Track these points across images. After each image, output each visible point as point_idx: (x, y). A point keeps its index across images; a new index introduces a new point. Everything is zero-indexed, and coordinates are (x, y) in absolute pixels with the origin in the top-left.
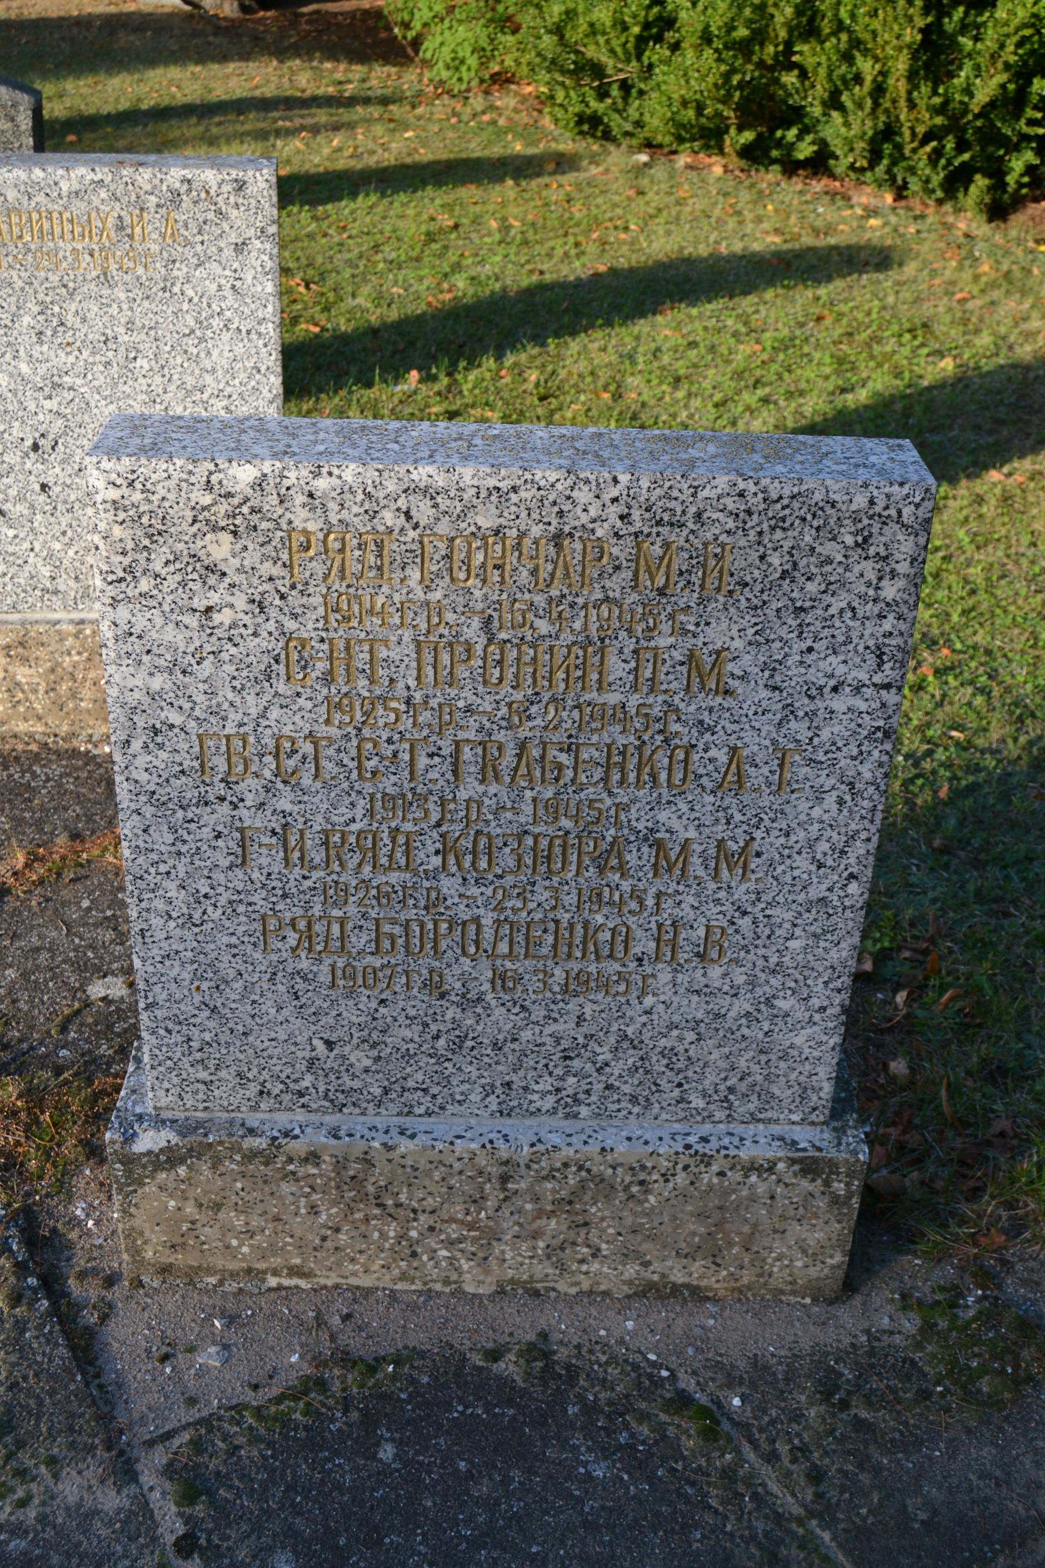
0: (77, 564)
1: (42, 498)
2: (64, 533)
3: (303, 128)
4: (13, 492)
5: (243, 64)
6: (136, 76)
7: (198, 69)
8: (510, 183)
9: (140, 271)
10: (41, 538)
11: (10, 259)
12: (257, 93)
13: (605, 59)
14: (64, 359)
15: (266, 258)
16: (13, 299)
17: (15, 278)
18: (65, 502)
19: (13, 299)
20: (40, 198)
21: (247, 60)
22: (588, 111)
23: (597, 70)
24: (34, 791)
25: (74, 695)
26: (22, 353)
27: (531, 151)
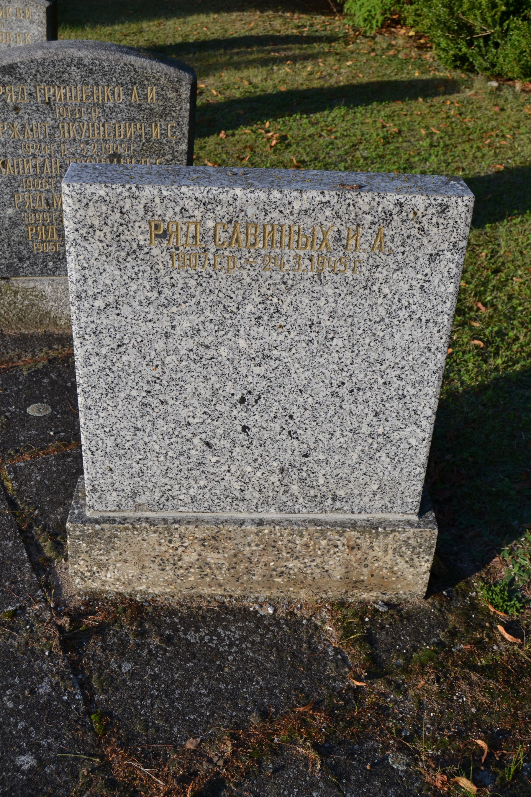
0: (262, 482)
1: (243, 436)
2: (255, 461)
3: (287, 58)
4: (219, 432)
5: (241, 14)
6: (182, 20)
7: (216, 16)
8: (421, 100)
9: (349, 273)
10: (237, 463)
11: (243, 261)
12: (253, 33)
13: (478, 24)
14: (275, 337)
15: (453, 266)
16: (241, 292)
17: (245, 276)
18: (260, 439)
19: (241, 292)
20: (275, 215)
21: (243, 11)
22: (460, 54)
23: (470, 29)
24: (222, 656)
25: (248, 571)
26: (242, 332)
27: (425, 77)
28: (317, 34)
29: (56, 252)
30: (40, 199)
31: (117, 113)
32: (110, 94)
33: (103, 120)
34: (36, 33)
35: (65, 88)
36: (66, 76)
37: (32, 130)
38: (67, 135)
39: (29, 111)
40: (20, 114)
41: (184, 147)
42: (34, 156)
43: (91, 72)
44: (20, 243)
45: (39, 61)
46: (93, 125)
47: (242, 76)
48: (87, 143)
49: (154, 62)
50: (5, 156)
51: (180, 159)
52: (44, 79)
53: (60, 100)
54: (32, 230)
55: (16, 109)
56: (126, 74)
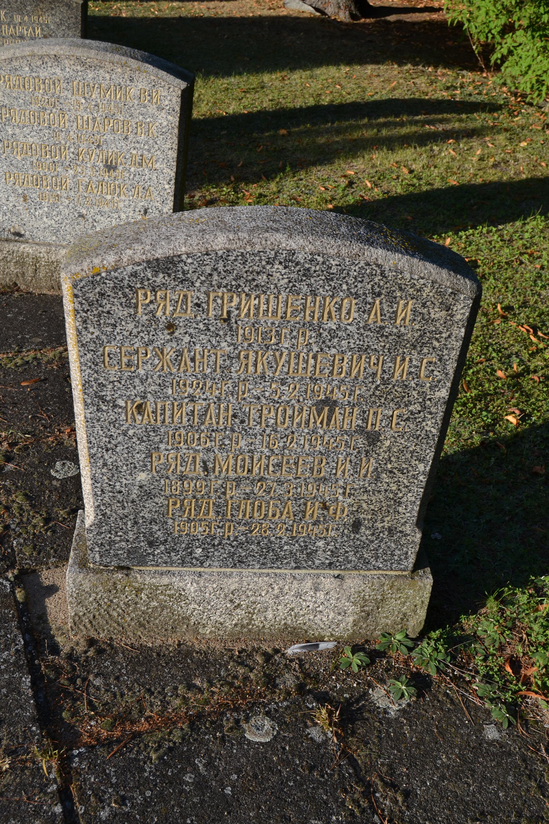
5: (376, 67)
6: (308, 72)
28: (472, 99)
29: (209, 535)
30: (195, 462)
31: (341, 339)
32: (333, 309)
33: (315, 349)
34: (165, 124)
35: (258, 297)
36: (262, 279)
37: (193, 360)
38: (251, 369)
39: (192, 331)
40: (176, 334)
41: (444, 393)
42: (192, 399)
43: (307, 273)
44: (153, 521)
45: (220, 253)
46: (298, 356)
47: (398, 159)
48: (283, 382)
49: (415, 260)
50: (144, 397)
51: (433, 410)
52: (225, 282)
53: (248, 315)
54: (175, 504)
55: (171, 327)
56: (366, 279)
